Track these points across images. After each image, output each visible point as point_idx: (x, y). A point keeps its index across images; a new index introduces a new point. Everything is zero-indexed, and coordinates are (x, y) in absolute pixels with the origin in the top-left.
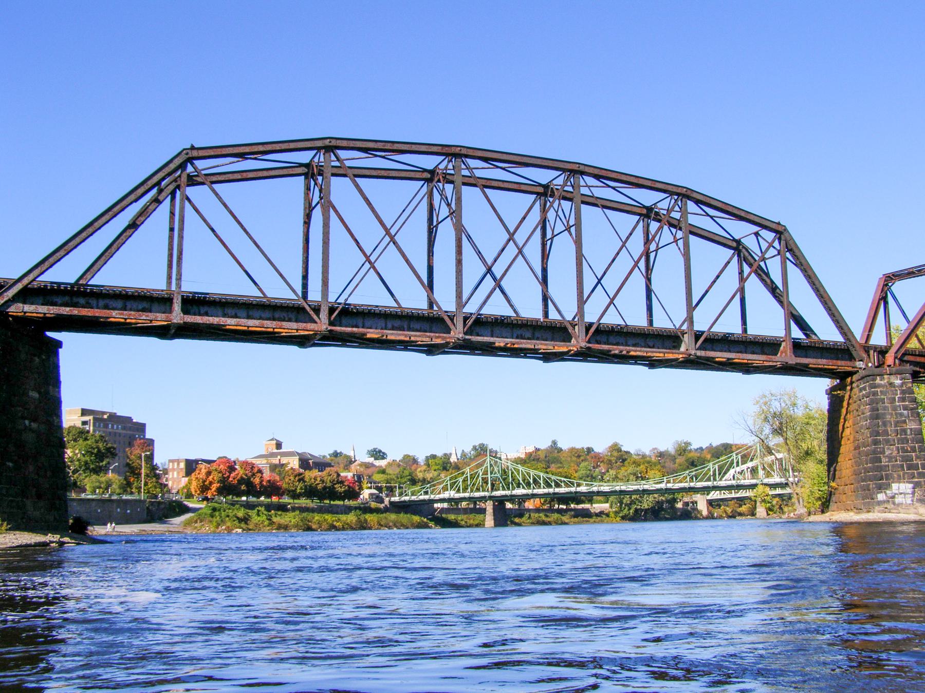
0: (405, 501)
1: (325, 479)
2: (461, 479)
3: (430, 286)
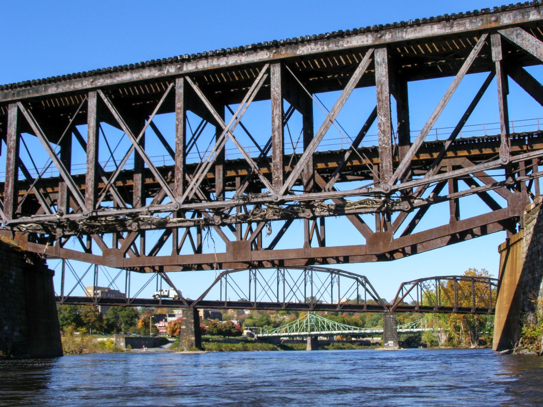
0: (265, 337)
1: (226, 326)
2: (294, 325)
3: (278, 298)
